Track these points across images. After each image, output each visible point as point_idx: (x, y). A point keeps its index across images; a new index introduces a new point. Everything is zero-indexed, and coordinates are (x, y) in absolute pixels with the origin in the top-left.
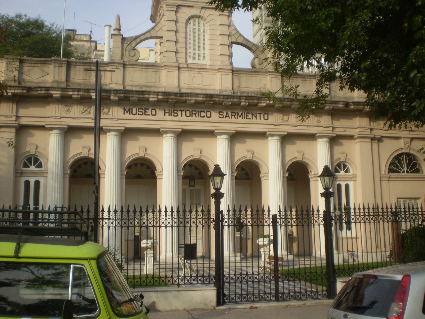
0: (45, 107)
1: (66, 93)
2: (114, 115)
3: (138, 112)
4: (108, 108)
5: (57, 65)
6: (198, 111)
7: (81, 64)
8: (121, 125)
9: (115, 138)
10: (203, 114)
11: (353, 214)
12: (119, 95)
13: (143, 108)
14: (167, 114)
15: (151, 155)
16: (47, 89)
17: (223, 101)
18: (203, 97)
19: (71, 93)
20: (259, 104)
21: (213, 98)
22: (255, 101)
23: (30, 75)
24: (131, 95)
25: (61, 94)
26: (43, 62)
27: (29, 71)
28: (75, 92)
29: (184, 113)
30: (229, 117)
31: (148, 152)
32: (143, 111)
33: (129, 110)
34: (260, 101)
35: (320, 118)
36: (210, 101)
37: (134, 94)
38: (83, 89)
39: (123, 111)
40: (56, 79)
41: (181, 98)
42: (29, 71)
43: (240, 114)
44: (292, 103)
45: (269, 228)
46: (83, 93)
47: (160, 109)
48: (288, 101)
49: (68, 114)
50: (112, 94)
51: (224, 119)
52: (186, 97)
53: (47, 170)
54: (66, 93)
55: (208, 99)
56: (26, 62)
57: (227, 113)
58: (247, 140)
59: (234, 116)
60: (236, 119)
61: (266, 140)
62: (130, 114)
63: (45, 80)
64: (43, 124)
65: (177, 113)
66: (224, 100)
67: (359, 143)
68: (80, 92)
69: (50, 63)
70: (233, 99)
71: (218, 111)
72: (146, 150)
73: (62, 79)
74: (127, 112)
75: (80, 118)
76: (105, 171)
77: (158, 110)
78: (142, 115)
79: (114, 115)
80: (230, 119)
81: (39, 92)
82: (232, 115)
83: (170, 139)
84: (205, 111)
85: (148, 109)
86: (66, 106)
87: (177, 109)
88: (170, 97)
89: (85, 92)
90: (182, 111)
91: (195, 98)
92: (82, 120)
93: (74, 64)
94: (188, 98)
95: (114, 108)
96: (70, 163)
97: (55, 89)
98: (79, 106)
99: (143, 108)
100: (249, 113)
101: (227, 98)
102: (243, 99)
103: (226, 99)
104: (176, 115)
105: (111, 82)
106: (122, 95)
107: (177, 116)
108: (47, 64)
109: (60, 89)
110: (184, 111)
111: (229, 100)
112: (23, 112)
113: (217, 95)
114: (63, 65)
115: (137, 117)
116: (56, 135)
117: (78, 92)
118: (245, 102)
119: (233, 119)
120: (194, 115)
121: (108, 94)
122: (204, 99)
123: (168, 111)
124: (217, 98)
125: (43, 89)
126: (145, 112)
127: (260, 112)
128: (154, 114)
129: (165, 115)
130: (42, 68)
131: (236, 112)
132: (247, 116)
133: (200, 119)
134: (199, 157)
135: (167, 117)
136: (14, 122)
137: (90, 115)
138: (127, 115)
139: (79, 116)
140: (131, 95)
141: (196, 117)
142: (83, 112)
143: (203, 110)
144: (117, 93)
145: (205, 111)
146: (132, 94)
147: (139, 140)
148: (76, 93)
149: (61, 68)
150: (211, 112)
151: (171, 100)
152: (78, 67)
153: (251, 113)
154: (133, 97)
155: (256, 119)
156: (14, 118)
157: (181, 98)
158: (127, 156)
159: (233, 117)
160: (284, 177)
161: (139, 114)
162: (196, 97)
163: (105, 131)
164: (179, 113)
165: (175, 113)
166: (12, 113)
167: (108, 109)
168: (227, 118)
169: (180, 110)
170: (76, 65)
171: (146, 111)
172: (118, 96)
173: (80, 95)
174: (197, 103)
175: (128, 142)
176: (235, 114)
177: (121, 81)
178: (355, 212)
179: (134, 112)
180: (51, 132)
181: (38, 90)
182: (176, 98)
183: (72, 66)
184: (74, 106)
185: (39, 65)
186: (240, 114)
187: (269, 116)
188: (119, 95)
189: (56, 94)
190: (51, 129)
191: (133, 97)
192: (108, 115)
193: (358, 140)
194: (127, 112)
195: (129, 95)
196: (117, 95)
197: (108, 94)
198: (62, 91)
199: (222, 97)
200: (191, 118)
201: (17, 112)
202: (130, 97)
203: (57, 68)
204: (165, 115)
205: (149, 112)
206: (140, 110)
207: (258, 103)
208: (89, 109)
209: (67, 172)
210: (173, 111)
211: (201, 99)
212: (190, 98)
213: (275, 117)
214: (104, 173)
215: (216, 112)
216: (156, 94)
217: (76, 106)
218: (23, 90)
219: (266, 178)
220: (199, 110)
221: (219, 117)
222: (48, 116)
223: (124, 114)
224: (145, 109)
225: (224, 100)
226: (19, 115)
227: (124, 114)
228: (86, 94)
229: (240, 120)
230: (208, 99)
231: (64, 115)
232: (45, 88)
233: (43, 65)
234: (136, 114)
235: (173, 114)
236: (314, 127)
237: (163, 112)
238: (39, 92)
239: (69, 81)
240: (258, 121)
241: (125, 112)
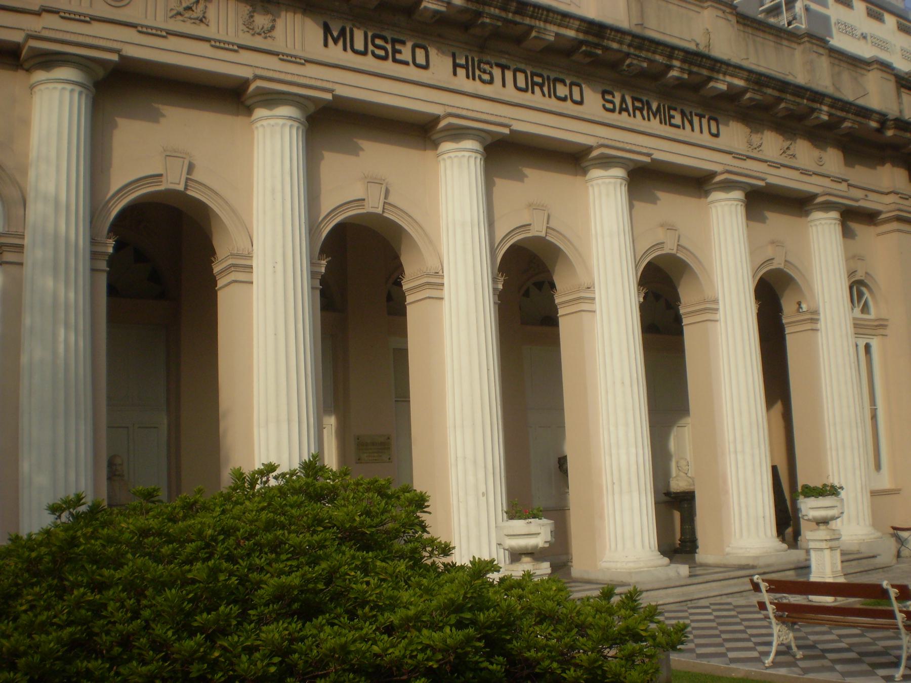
3: (371, 47)
6: (548, 78)
10: (562, 90)
13: (388, 35)
14: (461, 72)
17: (628, 55)
18: (578, 30)
20: (712, 84)
21: (603, 37)
22: (705, 72)
29: (509, 75)
30: (627, 110)
32: (389, 47)
33: (342, 33)
34: (715, 75)
36: (596, 46)
39: (320, 33)
41: (518, 19)
43: (654, 106)
44: (783, 96)
47: (439, 49)
48: (774, 88)
51: (615, 116)
52: (531, 17)
53: (22, 237)
55: (590, 38)
57: (623, 100)
58: (660, 194)
59: (641, 110)
60: (646, 123)
61: (803, 220)
62: (345, 49)
65: (491, 74)
66: (632, 51)
67: (895, 235)
70: (654, 52)
71: (600, 89)
72: (191, 168)
74: (336, 41)
76: (250, 257)
77: (433, 52)
78: (385, 58)
80: (631, 120)
82: (635, 108)
84: (568, 82)
85: (403, 43)
87: (488, 58)
88: (487, 9)
90: (504, 68)
91: (554, 28)
92: (173, 43)
94: (537, 23)
96: (114, 214)
99: (388, 35)
100: (675, 110)
101: (640, 48)
102: (677, 59)
103: (636, 48)
104: (486, 77)
107: (491, 82)
110: (508, 68)
111: (643, 54)
113: (618, 31)
115: (368, 62)
116: (69, 87)
118: (682, 70)
119: (638, 122)
120: (537, 89)
122: (581, 36)
123: (463, 62)
124: (613, 40)
126: (395, 51)
127: (699, 111)
128: (423, 63)
129: (455, 74)
131: (645, 99)
132: (395, 51)
133: (552, 104)
135: (462, 81)
137: (203, 26)
138: (336, 53)
139: (161, 22)
141: (544, 95)
142: (179, 14)
143: (562, 76)
145: (568, 82)
147: (162, 120)
150: (583, 86)
151: (488, 20)
153: (679, 110)
155: (693, 130)
157: (518, 19)
158: (116, 184)
159: (638, 113)
160: (313, 274)
161: (373, 54)
162: (560, 25)
164: (497, 72)
165: (485, 72)
168: (625, 114)
169: (498, 65)
171: (398, 47)
174: (732, 96)
175: (121, 122)
176: (642, 107)
179: (359, 45)
180: (40, 75)
182: (503, 15)
184: (283, 14)
186: (654, 106)
187: (722, 128)
190: (48, 60)
192: (269, 40)
193: (895, 225)
194: (336, 41)
199: (628, 39)
200: (529, 95)
204: (455, 74)
205: (406, 53)
206: (378, 42)
207: (710, 79)
208: (201, 6)
209: (103, 249)
210: (480, 62)
211: (571, 33)
212: (542, 24)
213: (734, 135)
214: (247, 262)
215: (594, 90)
219: (241, 276)
220: (553, 76)
221: (604, 106)
223: (326, 45)
224: (394, 41)
225: (632, 51)
227: (326, 45)
229: (654, 125)
230: (590, 38)
234: (364, 53)
235: (477, 73)
236: (814, 177)
237: (449, 62)
240: (696, 137)
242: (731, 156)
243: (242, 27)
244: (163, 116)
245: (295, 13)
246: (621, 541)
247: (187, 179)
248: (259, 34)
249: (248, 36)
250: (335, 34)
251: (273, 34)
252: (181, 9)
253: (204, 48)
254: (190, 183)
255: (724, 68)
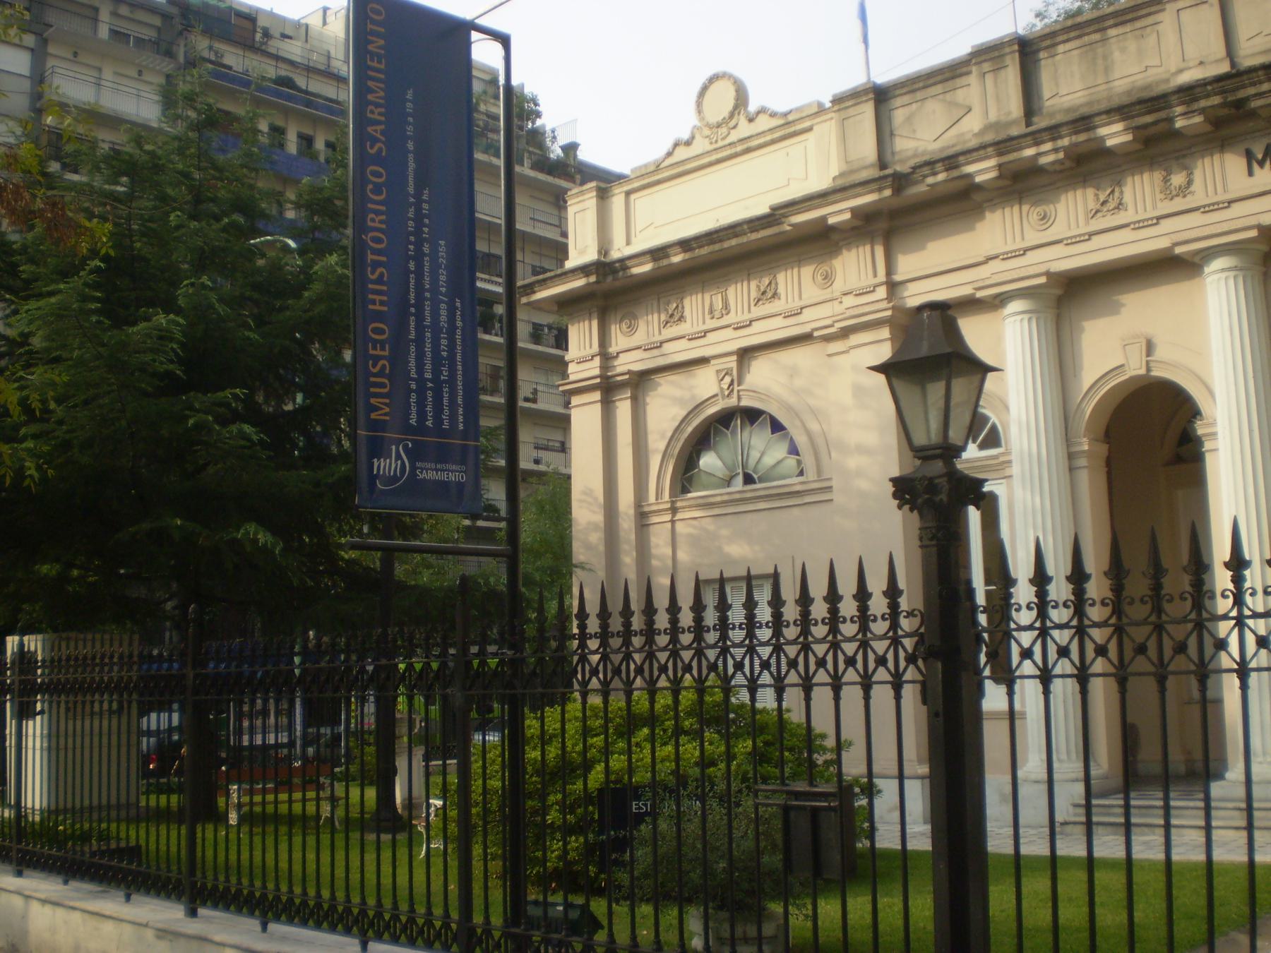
0: (972, 229)
1: (665, 262)
2: (1210, 188)
4: (1185, 168)
5: (986, 66)
7: (1072, 34)
8: (1031, 271)
9: (1240, 280)
11: (1025, 617)
12: (1203, 103)
15: (1170, 365)
16: (951, 161)
19: (1030, 152)
23: (914, 131)
24: (1251, 91)
25: (1000, 166)
26: (947, 75)
27: (909, 119)
28: (1043, 142)
31: (1160, 353)
35: (1049, 208)
37: (1261, 83)
38: (1067, 123)
40: (993, 116)
42: (909, 119)
45: (898, 697)
46: (1074, 139)
49: (1049, 232)
50: (1179, 110)
54: (665, 262)
56: (898, 92)
63: (963, 134)
64: (966, 291)
68: (1061, 137)
69: (964, 70)
72: (1150, 347)
73: (1009, 113)
75: (1091, 235)
79: (1210, 188)
81: (930, 180)
83: (1223, 283)
86: (1035, 204)
89: (1076, 133)
92: (1097, 241)
93: (1048, 42)
95: (1207, 161)
97: (832, 198)
98: (1079, 193)
105: (1182, 65)
106: (1216, 100)
108: (961, 75)
109: (990, 150)
112: (908, 264)
114: (1008, 60)
117: (1053, 139)
121: (1162, 115)
125: (939, 167)
130: (948, 96)
134: (1143, 371)
136: (884, 305)
137: (1122, 213)
140: (1251, 91)
144: (1196, 100)
146: (1254, 84)
147: (1123, 310)
148: (1048, 146)
149: (1003, 73)
152: (1061, 48)
154: (1260, 95)
156: (882, 292)
163: (1197, 259)
166: (875, 276)
167: (1184, 173)
170: (1054, 45)
172: (1202, 111)
173: (1065, 149)
177: (1219, 49)
178: (1042, 605)
181: (925, 176)
183: (1042, 55)
184: (1063, 198)
185: (938, 89)
188: (1203, 103)
189: (983, 170)
191: (1260, 95)
192: (1189, 197)
195: (1241, 94)
196: (1196, 106)
197: (1162, 115)
198: (1000, 154)
201: (890, 270)
202: (1247, 99)
203: (989, 79)
208: (1117, 194)
216: (648, 257)
217: (1070, 195)
218: (880, 190)
222: (981, 259)
223: (1251, 174)
226: (897, 278)
227: (1251, 174)
228: (1082, 137)
231: (1033, 238)
232: (943, 160)
233: (950, 84)
238: (930, 180)
239: (1040, 109)
241: (1255, 166)
242: (1128, 229)
243: (1159, 196)
244: (1123, 305)
245: (1142, 173)
246: (646, 909)
247: (1148, 362)
248: (1177, 195)
249: (1167, 203)
250: (1260, 156)
251: (1192, 189)
252: (1098, 206)
253: (683, 344)
254: (1152, 364)
255: (961, 159)
